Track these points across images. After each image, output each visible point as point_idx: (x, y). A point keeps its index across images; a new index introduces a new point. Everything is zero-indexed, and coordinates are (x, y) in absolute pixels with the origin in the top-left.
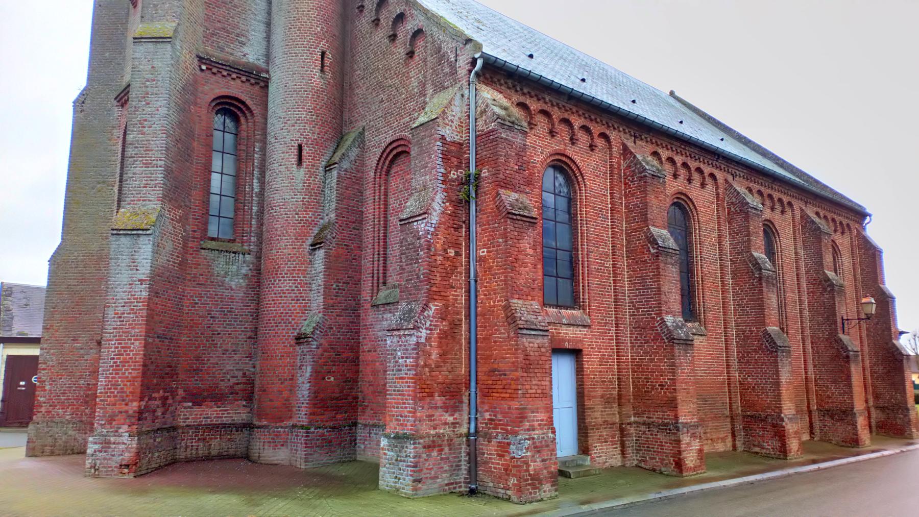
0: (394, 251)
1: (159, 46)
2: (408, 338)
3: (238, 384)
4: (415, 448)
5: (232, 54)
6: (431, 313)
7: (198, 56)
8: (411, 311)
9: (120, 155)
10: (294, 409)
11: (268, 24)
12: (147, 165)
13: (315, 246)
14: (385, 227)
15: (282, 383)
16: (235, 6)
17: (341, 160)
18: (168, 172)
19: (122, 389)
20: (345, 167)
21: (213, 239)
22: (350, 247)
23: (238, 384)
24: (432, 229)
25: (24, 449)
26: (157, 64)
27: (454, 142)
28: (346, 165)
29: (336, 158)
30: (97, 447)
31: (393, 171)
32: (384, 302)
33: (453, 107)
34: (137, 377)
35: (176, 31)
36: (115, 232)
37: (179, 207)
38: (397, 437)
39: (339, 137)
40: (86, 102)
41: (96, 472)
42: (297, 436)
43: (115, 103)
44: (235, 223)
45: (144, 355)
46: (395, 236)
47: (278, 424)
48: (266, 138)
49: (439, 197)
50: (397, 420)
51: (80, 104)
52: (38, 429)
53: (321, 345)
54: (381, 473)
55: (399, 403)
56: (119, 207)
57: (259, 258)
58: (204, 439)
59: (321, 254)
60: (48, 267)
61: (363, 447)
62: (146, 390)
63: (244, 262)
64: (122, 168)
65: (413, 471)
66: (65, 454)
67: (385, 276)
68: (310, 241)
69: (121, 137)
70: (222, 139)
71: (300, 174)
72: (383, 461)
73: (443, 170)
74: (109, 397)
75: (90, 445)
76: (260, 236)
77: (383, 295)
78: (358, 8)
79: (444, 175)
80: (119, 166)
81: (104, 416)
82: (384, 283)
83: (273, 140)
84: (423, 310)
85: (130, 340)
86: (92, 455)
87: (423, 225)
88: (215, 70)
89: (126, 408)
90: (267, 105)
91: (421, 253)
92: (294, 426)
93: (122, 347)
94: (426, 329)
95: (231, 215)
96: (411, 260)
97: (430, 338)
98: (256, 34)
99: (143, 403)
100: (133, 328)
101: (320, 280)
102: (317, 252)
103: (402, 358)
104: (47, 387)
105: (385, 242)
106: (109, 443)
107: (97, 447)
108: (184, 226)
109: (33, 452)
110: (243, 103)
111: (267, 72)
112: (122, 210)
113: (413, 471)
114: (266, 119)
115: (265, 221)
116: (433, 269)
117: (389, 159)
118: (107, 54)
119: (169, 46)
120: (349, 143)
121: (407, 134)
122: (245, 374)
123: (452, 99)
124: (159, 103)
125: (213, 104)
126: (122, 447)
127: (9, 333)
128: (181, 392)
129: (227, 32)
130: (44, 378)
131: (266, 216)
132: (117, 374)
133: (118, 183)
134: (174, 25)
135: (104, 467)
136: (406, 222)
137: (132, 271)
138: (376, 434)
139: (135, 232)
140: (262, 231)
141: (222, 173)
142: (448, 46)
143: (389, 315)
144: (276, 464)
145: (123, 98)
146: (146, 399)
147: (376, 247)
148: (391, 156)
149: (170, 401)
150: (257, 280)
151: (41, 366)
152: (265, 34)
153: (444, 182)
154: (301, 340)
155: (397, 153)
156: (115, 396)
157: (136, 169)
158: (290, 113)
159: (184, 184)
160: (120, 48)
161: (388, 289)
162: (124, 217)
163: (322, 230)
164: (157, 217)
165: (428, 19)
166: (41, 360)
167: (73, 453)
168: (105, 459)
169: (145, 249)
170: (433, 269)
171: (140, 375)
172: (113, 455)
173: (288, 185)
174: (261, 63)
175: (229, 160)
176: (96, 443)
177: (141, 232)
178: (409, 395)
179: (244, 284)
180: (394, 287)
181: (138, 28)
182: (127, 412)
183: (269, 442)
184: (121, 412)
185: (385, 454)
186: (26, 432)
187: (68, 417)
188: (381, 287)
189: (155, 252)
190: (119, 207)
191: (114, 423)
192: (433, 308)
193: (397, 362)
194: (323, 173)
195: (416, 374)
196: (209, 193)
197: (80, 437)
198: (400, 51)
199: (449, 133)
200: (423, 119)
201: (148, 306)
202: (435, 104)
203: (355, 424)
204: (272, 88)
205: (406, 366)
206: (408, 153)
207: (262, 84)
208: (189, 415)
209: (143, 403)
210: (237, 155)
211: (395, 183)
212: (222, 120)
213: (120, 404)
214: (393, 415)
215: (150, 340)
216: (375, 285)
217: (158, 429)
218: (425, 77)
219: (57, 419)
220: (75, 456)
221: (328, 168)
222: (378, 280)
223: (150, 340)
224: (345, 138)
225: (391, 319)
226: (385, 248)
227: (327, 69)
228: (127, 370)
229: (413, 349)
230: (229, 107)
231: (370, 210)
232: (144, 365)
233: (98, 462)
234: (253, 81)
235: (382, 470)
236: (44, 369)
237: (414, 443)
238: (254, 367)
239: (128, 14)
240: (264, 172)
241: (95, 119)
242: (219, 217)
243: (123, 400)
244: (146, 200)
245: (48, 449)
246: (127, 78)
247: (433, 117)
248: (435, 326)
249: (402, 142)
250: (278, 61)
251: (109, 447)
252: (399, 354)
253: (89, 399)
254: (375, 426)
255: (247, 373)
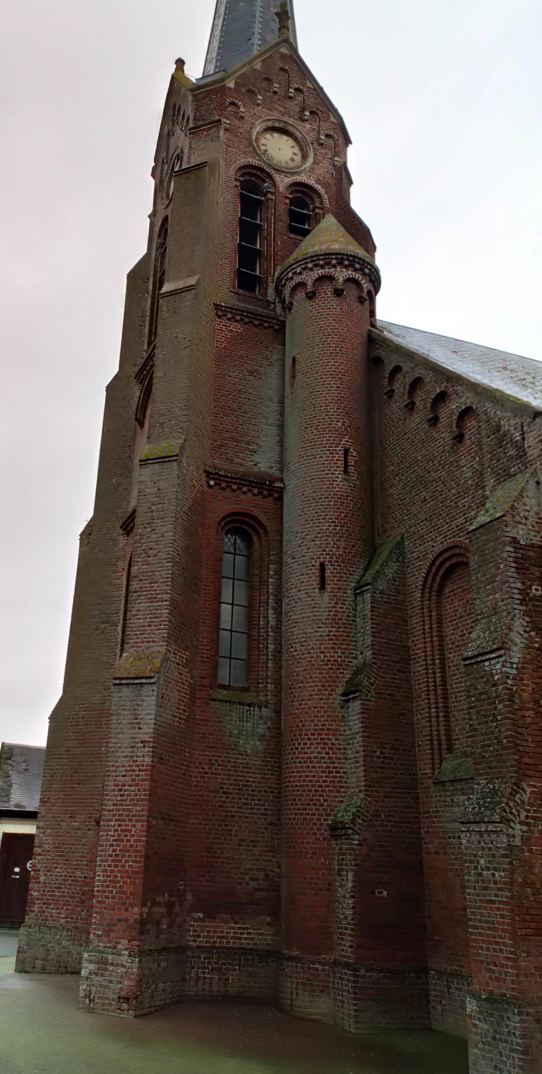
0: (459, 703)
1: (165, 465)
2: (493, 836)
3: (259, 890)
4: (521, 1021)
5: (241, 465)
6: (526, 798)
7: (205, 472)
8: (494, 792)
9: (124, 589)
10: (335, 937)
11: (281, 427)
12: (152, 599)
13: (349, 694)
14: (443, 668)
15: (316, 894)
16: (245, 412)
17: (375, 579)
18: (174, 606)
19: (121, 887)
20: (380, 588)
21: (224, 687)
22: (395, 693)
23: (259, 890)
24: (514, 671)
25: (13, 960)
26: (163, 485)
27: (532, 545)
28: (381, 585)
29: (368, 578)
30: (92, 967)
31: (447, 590)
32: (452, 777)
33: (526, 500)
34: (138, 872)
35: (182, 447)
36: (117, 682)
37: (186, 648)
38: (491, 999)
39: (371, 552)
40: (93, 533)
41: (90, 1004)
42: (341, 978)
43: (121, 531)
44: (250, 665)
45: (147, 842)
46: (458, 682)
47: (314, 958)
48: (282, 558)
49: (519, 624)
50: (490, 970)
51: (87, 536)
52: (29, 934)
53: (365, 840)
54: (471, 1058)
55: (490, 943)
56: (122, 650)
57: (278, 712)
58: (219, 970)
59: (356, 706)
60: (48, 724)
61: (439, 1008)
62: (148, 894)
63: (261, 718)
64: (126, 604)
65: (523, 1060)
66: (57, 973)
67: (449, 740)
68: (340, 690)
69: (126, 568)
70: (232, 563)
71: (325, 600)
72: (473, 1037)
73: (519, 585)
74: (107, 897)
75: (85, 964)
76: (278, 683)
77: (449, 765)
78: (386, 393)
79: (521, 591)
80: (123, 602)
81: (101, 924)
82: (450, 750)
83: (290, 560)
84: (513, 793)
85: (130, 820)
86: (87, 978)
87: (498, 666)
88: (224, 485)
89: (126, 915)
90: (282, 518)
91: (500, 706)
92: (336, 963)
93: (122, 831)
94: (521, 823)
95: (244, 657)
96: (485, 716)
97: (529, 839)
98: (267, 439)
99: (146, 910)
100: (135, 805)
101: (357, 744)
102: (350, 704)
103: (488, 869)
104: (42, 879)
105: (445, 691)
106: (106, 963)
107: (92, 967)
108: (190, 671)
109: (23, 968)
110: (256, 519)
111: (282, 480)
112: (125, 655)
113: (523, 1060)
114: (282, 535)
115: (283, 663)
116: (520, 730)
117: (440, 574)
118: (114, 481)
119: (175, 464)
120: (384, 556)
121: (463, 540)
122: (267, 876)
123: (523, 489)
124: (165, 529)
125: (223, 523)
126: (121, 970)
127: (6, 805)
128: (189, 896)
129: (237, 441)
130: (39, 866)
131: (285, 657)
132: (116, 866)
133: (122, 622)
134: (181, 441)
135: (100, 998)
136: (473, 662)
137: (137, 722)
138: (459, 990)
139: (135, 681)
140: (280, 676)
141: (233, 604)
142: (509, 424)
143: (462, 798)
144: (314, 1021)
145: (128, 526)
146: (149, 904)
147: (432, 697)
148: (442, 571)
149: (177, 909)
150: (277, 743)
151: (37, 850)
152: (278, 438)
153: (523, 602)
154: (338, 832)
155: (450, 567)
156: (114, 897)
157: (140, 605)
158: (310, 525)
159: (191, 623)
160: (127, 471)
161: (456, 757)
162: (126, 663)
163: (355, 674)
164: (162, 661)
165: (478, 394)
166: (37, 841)
167: (67, 972)
168: (101, 986)
169: (150, 699)
170: (520, 730)
171: (142, 870)
172: (110, 982)
173: (311, 614)
174: (275, 472)
175: (241, 588)
176: (91, 962)
177: (144, 681)
178: (504, 931)
179: (261, 748)
180: (466, 755)
181: (144, 449)
182: (126, 920)
183: (304, 984)
184: (120, 920)
185: (475, 1025)
186: (17, 935)
187: (62, 921)
188: (445, 754)
189: (158, 706)
190: (122, 650)
191: (112, 935)
192: (528, 790)
193: (480, 875)
194: (353, 598)
195: (512, 897)
196: (218, 629)
197: (74, 949)
198: (445, 435)
199: (521, 533)
200: (483, 518)
201: (151, 775)
202: (499, 498)
203: (425, 970)
204: (287, 498)
205: (495, 882)
206: (466, 564)
207: (276, 495)
208: (201, 931)
209: (146, 910)
210: (249, 580)
211: (452, 606)
212: (232, 541)
213: (119, 909)
214: (482, 962)
215: (154, 822)
216: (436, 752)
217: (163, 949)
218: (481, 464)
219: (50, 923)
220: (68, 977)
221: (358, 591)
222: (440, 744)
223: (154, 822)
224: (378, 551)
225: (466, 803)
226: (446, 699)
227: (351, 469)
228: (127, 861)
229: (504, 856)
230: (241, 526)
231: (419, 645)
232: (147, 857)
233: (94, 989)
234: (265, 493)
235: (473, 1051)
236: (39, 855)
237: (520, 1013)
238: (279, 867)
239: (134, 436)
240: (281, 600)
241: (101, 551)
242: (231, 658)
243: (123, 904)
244: (150, 643)
245: (39, 963)
246: (133, 503)
247: (498, 515)
248: (534, 818)
249: (457, 551)
250: (292, 468)
251: (106, 970)
252: (482, 861)
253: (85, 898)
254: (454, 975)
255: (271, 874)
